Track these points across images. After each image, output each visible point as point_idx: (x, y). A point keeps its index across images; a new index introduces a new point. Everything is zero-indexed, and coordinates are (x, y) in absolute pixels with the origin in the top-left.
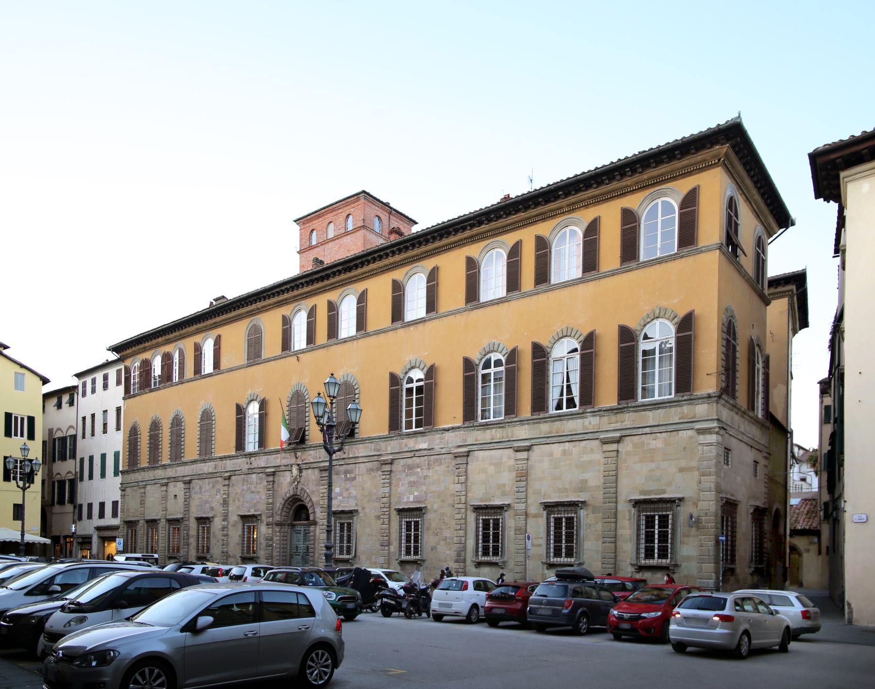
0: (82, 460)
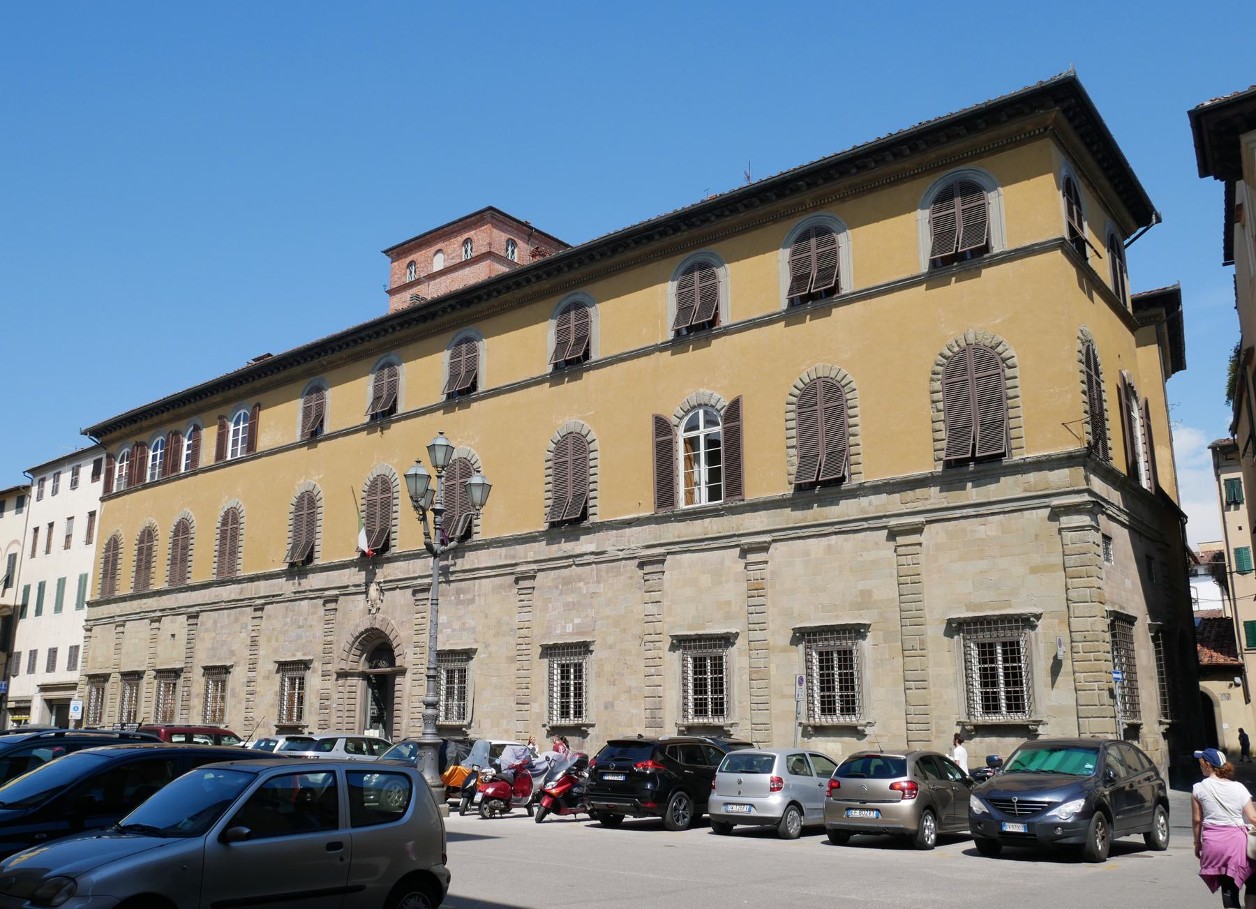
0: (27, 589)
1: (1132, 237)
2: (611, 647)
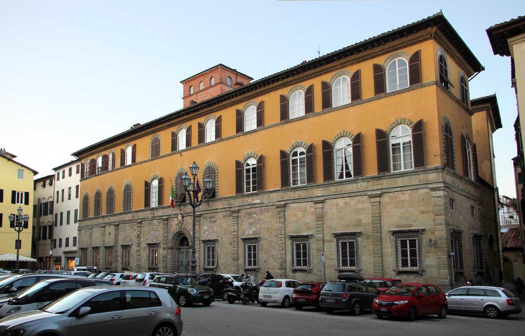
0: (56, 215)
1: (472, 76)
2: (266, 239)
